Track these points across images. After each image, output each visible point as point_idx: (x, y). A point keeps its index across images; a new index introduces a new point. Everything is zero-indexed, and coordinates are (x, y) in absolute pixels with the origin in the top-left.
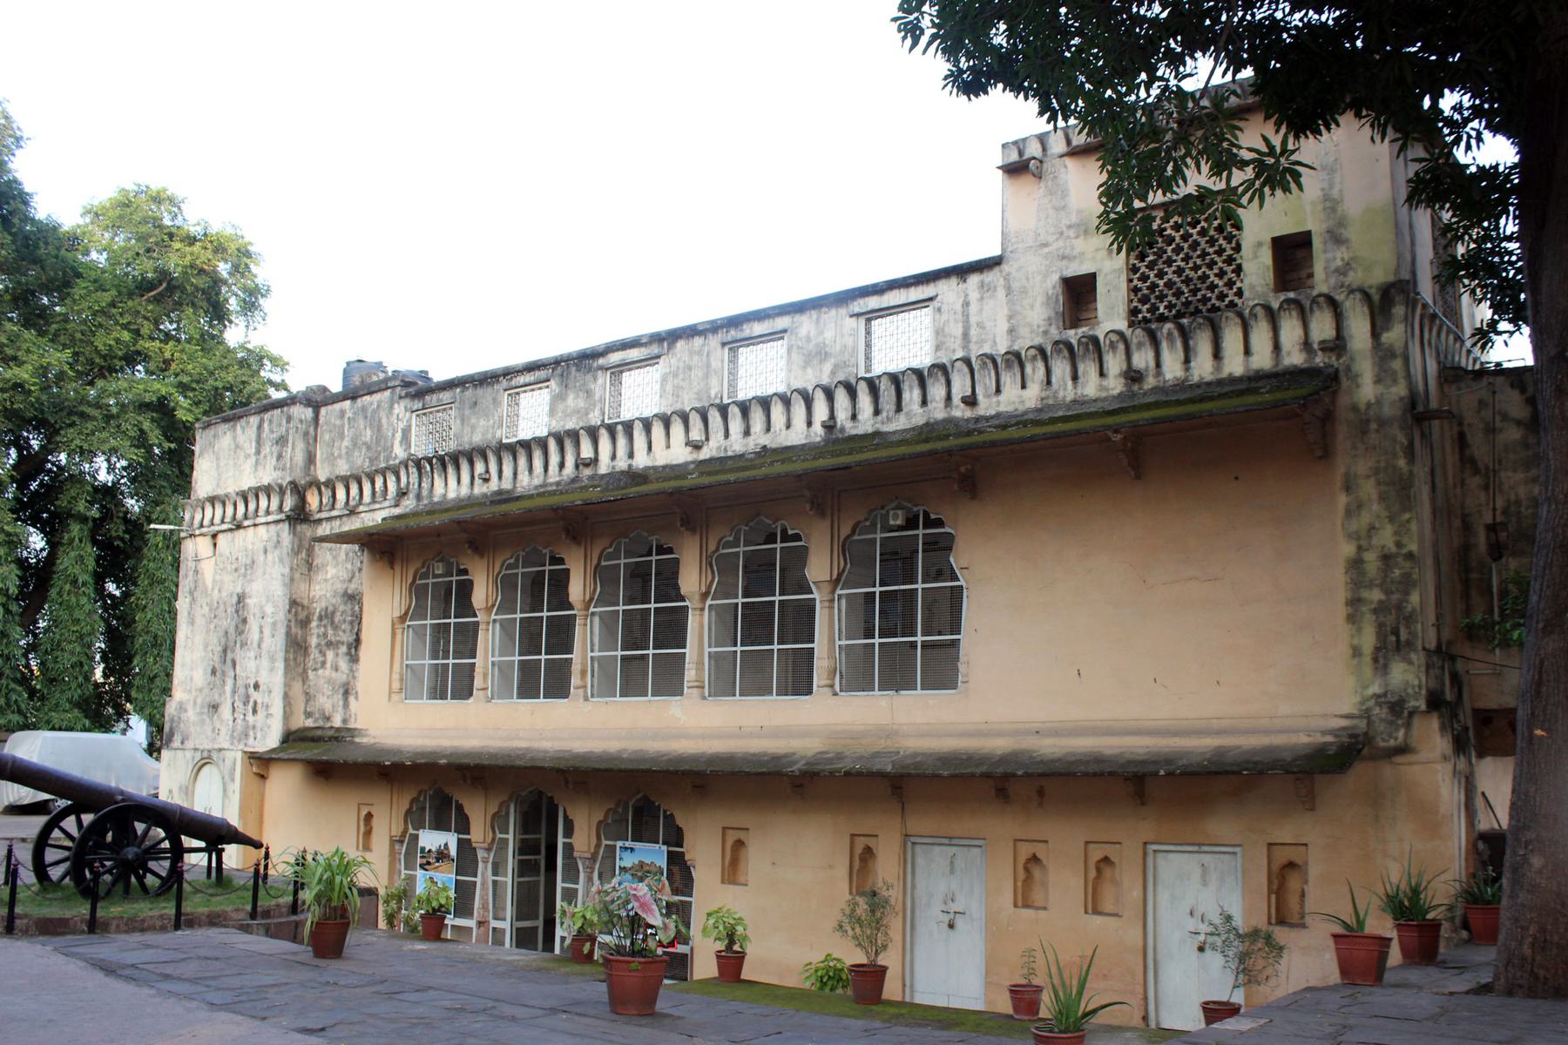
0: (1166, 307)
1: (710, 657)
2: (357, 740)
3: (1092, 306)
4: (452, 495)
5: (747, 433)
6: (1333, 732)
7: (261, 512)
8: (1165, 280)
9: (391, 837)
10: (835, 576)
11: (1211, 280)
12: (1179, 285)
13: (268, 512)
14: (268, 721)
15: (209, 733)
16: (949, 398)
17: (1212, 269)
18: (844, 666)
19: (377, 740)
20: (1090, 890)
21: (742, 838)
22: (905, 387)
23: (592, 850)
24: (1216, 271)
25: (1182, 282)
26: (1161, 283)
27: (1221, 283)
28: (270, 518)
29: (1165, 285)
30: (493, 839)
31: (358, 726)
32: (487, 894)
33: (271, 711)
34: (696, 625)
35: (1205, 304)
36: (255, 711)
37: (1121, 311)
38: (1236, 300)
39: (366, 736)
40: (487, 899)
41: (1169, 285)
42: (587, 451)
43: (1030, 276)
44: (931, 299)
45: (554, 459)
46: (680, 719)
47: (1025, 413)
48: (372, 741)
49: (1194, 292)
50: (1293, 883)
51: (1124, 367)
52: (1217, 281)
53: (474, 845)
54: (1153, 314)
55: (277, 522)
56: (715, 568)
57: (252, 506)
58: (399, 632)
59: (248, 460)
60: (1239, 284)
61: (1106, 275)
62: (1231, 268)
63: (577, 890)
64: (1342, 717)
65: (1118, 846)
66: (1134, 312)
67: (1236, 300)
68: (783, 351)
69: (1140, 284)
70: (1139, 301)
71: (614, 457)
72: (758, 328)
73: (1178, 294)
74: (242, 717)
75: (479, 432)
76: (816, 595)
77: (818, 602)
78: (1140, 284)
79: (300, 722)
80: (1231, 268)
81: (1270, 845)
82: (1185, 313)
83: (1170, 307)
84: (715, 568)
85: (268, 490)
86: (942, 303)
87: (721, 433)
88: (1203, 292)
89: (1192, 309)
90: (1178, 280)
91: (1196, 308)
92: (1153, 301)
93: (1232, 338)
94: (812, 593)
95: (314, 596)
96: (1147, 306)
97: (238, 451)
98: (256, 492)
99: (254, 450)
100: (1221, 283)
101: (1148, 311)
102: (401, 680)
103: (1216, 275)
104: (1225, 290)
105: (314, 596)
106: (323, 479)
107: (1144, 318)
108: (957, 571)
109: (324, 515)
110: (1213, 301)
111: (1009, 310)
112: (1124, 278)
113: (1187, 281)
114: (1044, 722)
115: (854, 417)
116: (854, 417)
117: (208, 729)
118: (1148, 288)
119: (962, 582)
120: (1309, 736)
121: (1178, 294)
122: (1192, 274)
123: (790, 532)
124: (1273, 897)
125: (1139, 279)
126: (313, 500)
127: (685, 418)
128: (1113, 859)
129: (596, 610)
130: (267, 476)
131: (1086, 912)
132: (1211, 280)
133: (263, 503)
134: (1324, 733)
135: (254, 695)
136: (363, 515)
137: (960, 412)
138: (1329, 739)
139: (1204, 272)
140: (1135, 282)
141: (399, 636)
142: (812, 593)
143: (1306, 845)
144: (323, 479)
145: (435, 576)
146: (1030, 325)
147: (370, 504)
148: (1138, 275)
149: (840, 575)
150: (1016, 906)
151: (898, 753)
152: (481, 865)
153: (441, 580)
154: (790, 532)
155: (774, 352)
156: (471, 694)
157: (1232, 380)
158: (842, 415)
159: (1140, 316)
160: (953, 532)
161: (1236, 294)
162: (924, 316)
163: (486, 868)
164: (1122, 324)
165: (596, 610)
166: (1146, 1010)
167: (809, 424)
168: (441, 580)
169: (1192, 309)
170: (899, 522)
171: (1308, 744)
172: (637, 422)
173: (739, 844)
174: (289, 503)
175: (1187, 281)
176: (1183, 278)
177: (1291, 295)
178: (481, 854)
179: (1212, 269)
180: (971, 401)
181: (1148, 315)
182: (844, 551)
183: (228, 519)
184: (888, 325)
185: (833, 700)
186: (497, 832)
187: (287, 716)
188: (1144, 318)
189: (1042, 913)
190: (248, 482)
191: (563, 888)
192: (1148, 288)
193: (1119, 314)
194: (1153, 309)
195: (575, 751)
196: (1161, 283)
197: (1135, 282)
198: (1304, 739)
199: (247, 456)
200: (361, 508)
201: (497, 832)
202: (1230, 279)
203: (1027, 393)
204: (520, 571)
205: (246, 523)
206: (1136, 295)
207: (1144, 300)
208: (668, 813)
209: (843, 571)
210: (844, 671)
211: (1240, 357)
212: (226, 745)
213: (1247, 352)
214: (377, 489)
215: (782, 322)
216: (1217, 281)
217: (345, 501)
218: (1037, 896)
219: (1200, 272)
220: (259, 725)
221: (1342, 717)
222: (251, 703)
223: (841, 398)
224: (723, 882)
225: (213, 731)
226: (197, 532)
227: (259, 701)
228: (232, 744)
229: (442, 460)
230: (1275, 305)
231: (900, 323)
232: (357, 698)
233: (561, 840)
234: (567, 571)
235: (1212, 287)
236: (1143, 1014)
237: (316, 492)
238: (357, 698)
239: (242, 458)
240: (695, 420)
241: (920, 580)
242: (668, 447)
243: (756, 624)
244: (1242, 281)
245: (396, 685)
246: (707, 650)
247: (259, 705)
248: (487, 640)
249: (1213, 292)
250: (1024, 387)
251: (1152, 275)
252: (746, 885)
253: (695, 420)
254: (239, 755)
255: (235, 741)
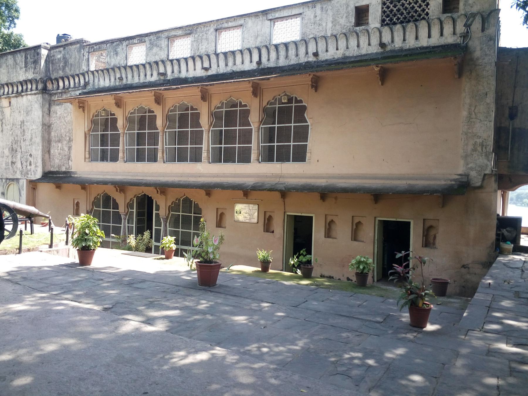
0: (396, 19)
1: (212, 148)
2: (73, 176)
3: (365, 18)
4: (142, 81)
5: (226, 65)
6: (454, 180)
7: (29, 90)
8: (397, 8)
9: (87, 211)
10: (89, 129)
11: (416, 8)
12: (402, 10)
13: (31, 90)
14: (36, 168)
15: (12, 173)
16: (307, 53)
17: (416, 4)
18: (263, 153)
19: (81, 176)
20: (353, 232)
21: (271, 215)
22: (290, 48)
23: (167, 215)
24: (418, 5)
25: (404, 9)
26: (395, 9)
27: (420, 10)
28: (33, 92)
29: (397, 10)
30: (128, 212)
31: (72, 170)
32: (126, 231)
33: (38, 165)
34: (207, 137)
35: (412, 18)
36: (30, 165)
37: (378, 20)
38: (426, 17)
39: (76, 174)
40: (126, 232)
41: (398, 10)
42: (162, 70)
43: (342, 6)
44: (301, 14)
45: (149, 73)
46: (201, 170)
47: (338, 59)
48: (79, 176)
49: (408, 13)
50: (432, 233)
51: (379, 42)
52: (418, 9)
53: (120, 213)
54: (391, 21)
55: (35, 94)
56: (214, 116)
57: (25, 88)
58: (88, 136)
59: (22, 70)
60: (427, 10)
61: (373, 5)
62: (424, 4)
63: (161, 229)
64: (457, 175)
65: (364, 218)
66: (383, 21)
67: (426, 17)
68: (189, 42)
69: (386, 10)
70: (385, 16)
71: (173, 72)
72: (285, 13)
73: (402, 14)
74: (25, 167)
75: (116, 61)
76: (253, 127)
77: (253, 130)
78: (386, 10)
79: (47, 170)
80: (424, 4)
81: (424, 219)
82: (404, 21)
83: (398, 19)
84: (214, 116)
85: (31, 81)
86: (305, 15)
87: (216, 65)
88: (412, 13)
89: (407, 20)
90: (402, 8)
91: (409, 20)
92: (391, 16)
93: (423, 32)
94: (251, 126)
95: (52, 122)
96: (389, 18)
97: (17, 66)
98: (26, 82)
99: (24, 66)
100: (420, 10)
101: (389, 20)
102: (89, 154)
103: (418, 7)
104: (421, 13)
105: (52, 122)
106: (53, 78)
107: (387, 23)
108: (251, 123)
109: (54, 92)
110: (416, 17)
111: (333, 19)
112: (380, 6)
113: (406, 9)
114: (339, 174)
115: (269, 60)
116: (269, 60)
117: (11, 171)
118: (389, 11)
119: (203, 129)
120: (445, 181)
121: (402, 14)
122: (408, 6)
123: (243, 104)
124: (424, 238)
125: (386, 8)
126: (49, 86)
127: (201, 57)
128: (362, 222)
129: (127, 132)
130: (30, 75)
131: (352, 240)
132: (416, 8)
133: (29, 86)
134: (451, 180)
135: (31, 159)
136: (71, 92)
137: (312, 59)
138: (453, 183)
139: (413, 6)
140: (385, 9)
141: (88, 138)
142: (251, 126)
143: (438, 220)
144: (53, 78)
145: (101, 116)
146: (341, 25)
147: (73, 88)
148: (386, 6)
149: (262, 120)
150: (325, 237)
151: (285, 184)
152: (123, 220)
153: (104, 117)
154: (243, 104)
155: (179, 43)
156: (118, 160)
157: (422, 48)
158: (264, 59)
159: (385, 22)
160: (306, 105)
161: (425, 14)
162: (297, 21)
163: (125, 221)
164: (378, 25)
165: (127, 132)
166: (373, 274)
167: (251, 62)
168: (104, 117)
169: (407, 20)
170: (286, 101)
171: (446, 184)
172: (182, 59)
173: (359, 223)
174: (40, 86)
175: (406, 9)
176: (404, 7)
177: (449, 15)
178: (122, 217)
179: (416, 4)
180: (316, 54)
181: (389, 22)
182: (264, 112)
183: (15, 92)
184: (188, 40)
185: (259, 165)
186: (129, 209)
187: (43, 167)
188: (387, 23)
189: (335, 240)
190: (21, 79)
191: (155, 228)
192: (389, 11)
193: (377, 21)
194: (391, 20)
195: (229, 182)
196: (395, 9)
197: (385, 9)
198: (443, 183)
199: (21, 68)
200: (70, 89)
201: (129, 209)
202: (423, 8)
203: (338, 52)
204: (136, 115)
205: (23, 94)
206: (384, 14)
207: (388, 16)
208: (196, 203)
209: (263, 118)
210: (263, 155)
211: (426, 39)
212: (19, 177)
213: (429, 36)
214: (76, 82)
215: (241, 22)
216: (418, 9)
217: (63, 86)
218: (333, 234)
219: (411, 5)
220: (32, 170)
221: (457, 175)
222: (29, 162)
223: (264, 52)
224: (216, 227)
225: (14, 172)
226: (30, 93)
227: (32, 161)
228: (22, 177)
229: (108, 70)
230: (443, 19)
231: (230, 33)
232: (71, 161)
233: (154, 212)
234: (155, 116)
235: (416, 11)
236: (372, 276)
237: (51, 83)
238: (71, 161)
239: (19, 69)
240: (205, 58)
241: (238, 126)
242: (195, 70)
243: (182, 138)
244: (429, 9)
245: (87, 156)
246: (211, 146)
247: (32, 162)
248: (123, 140)
249: (416, 13)
250: (337, 49)
251: (391, 6)
252: (225, 228)
253: (205, 58)
254: (25, 181)
255: (23, 176)
